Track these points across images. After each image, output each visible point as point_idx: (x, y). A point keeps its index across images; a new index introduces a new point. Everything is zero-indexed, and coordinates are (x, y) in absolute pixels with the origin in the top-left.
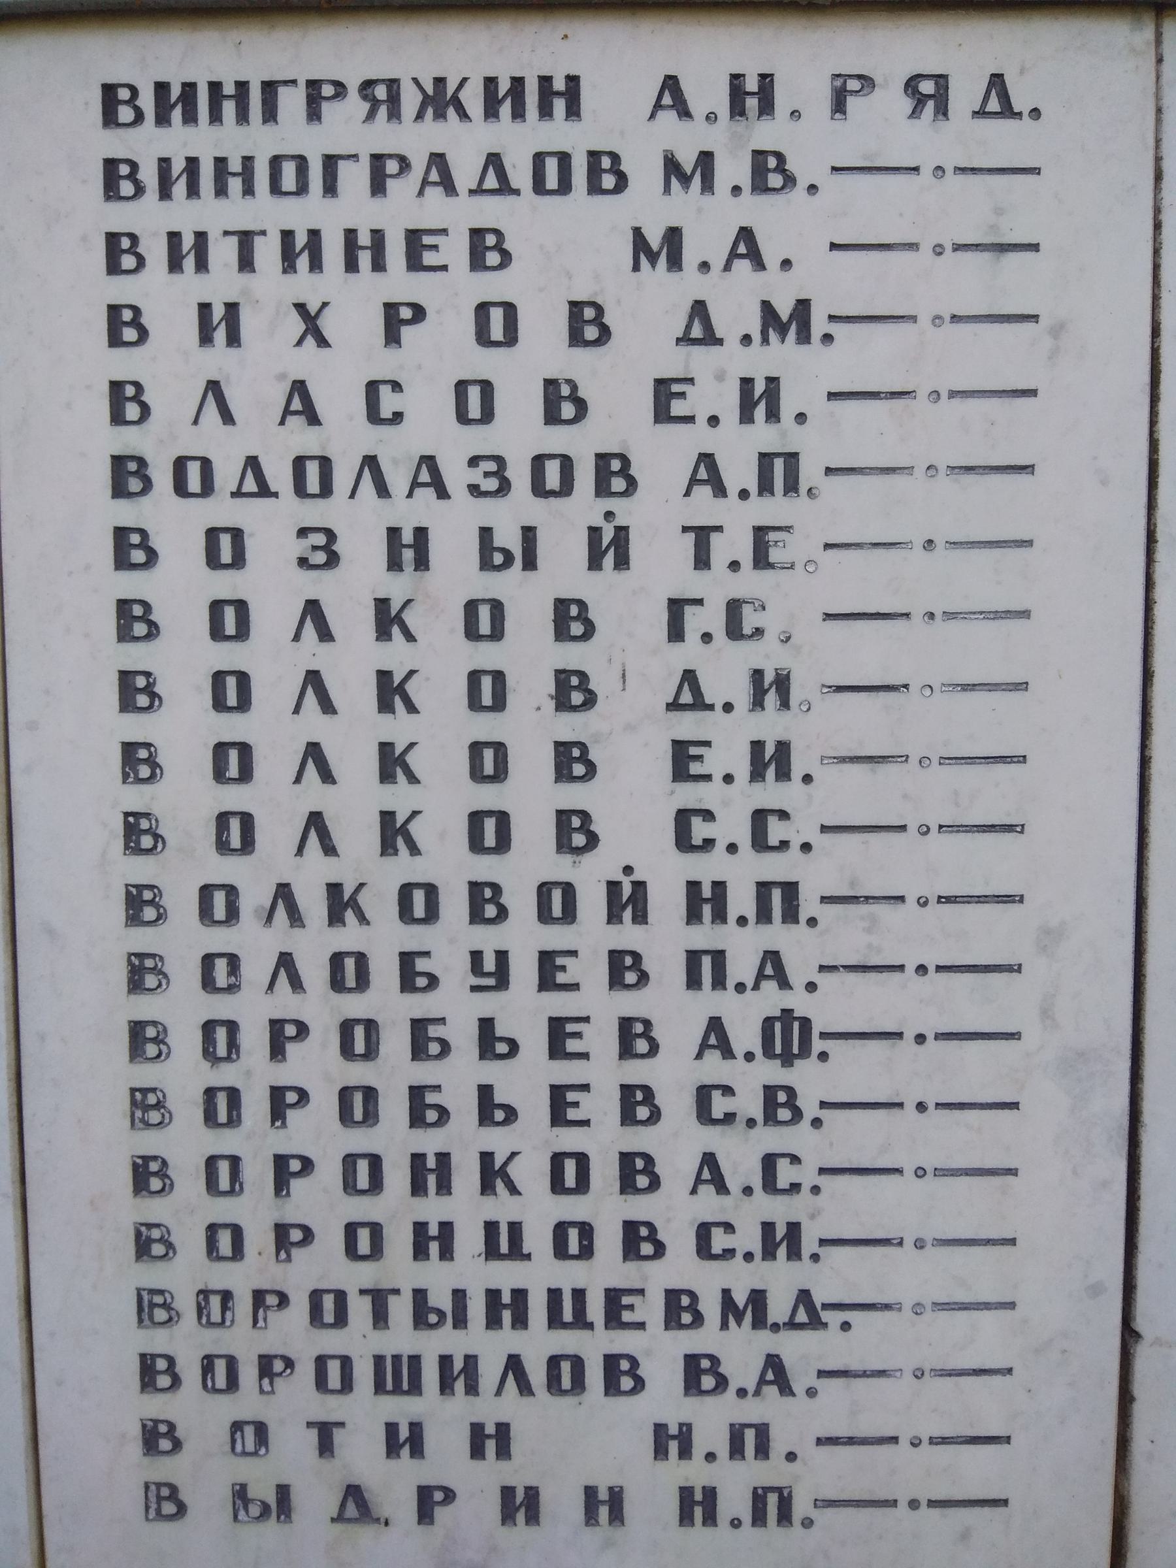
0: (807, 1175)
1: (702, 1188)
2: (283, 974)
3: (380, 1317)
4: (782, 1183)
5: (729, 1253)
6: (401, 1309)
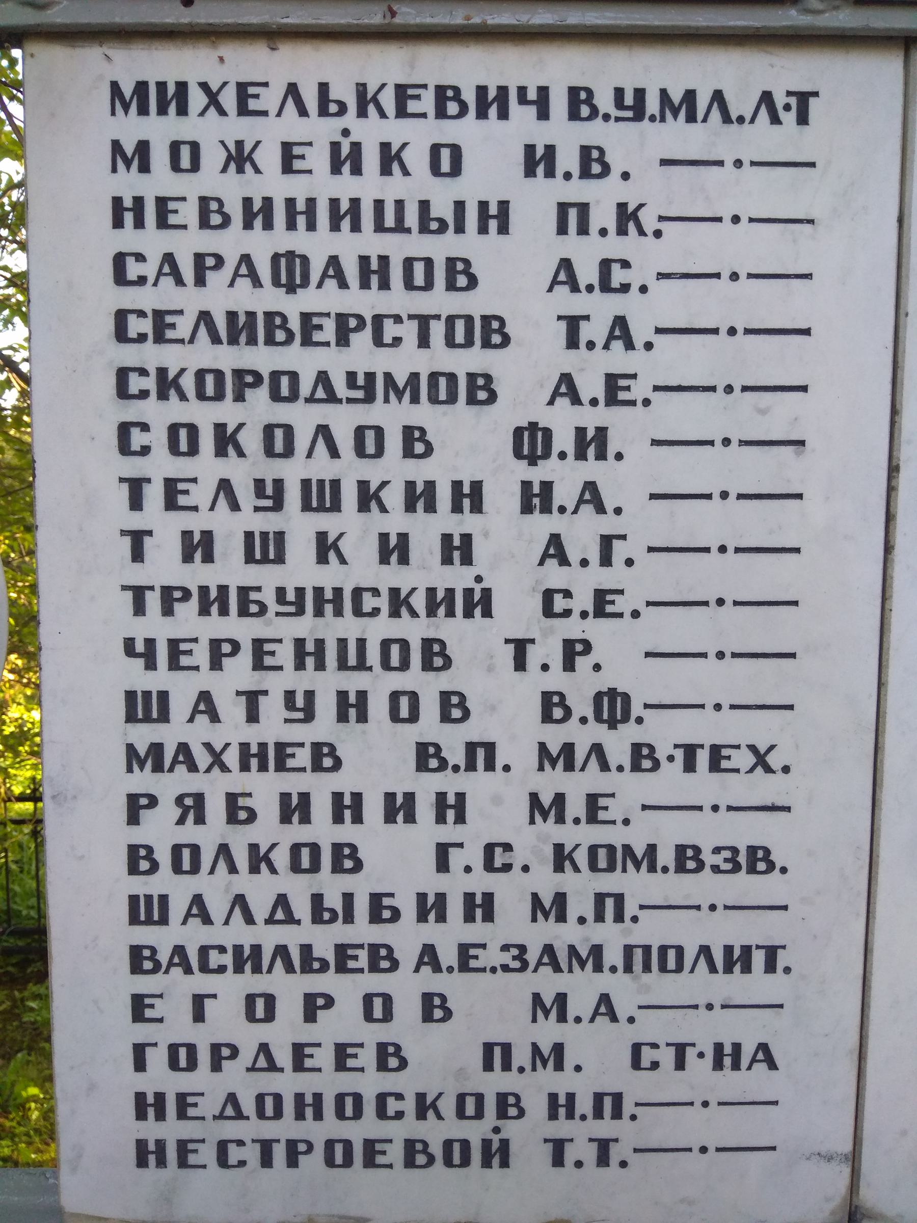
0: (633, 277)
1: (559, 401)
4: (615, 284)
5: (567, 613)
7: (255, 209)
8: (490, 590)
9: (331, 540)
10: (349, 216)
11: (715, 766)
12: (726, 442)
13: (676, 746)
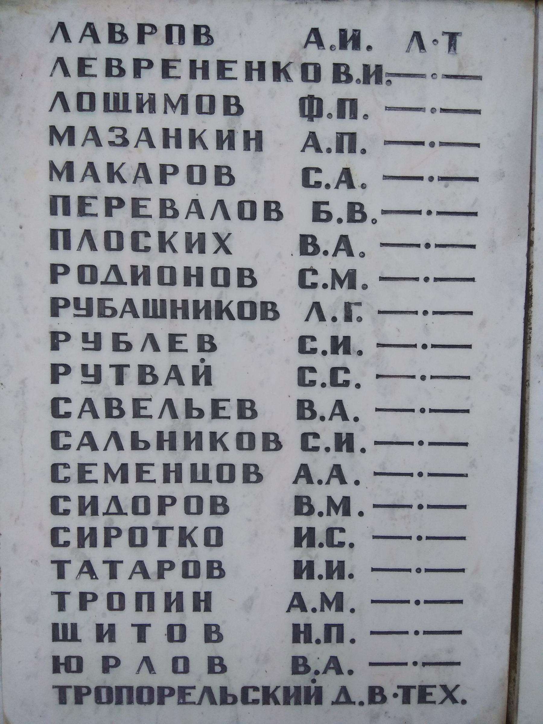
3: (162, 543)
7: (201, 308)
9: (282, 66)
12: (421, 443)
13: (399, 687)
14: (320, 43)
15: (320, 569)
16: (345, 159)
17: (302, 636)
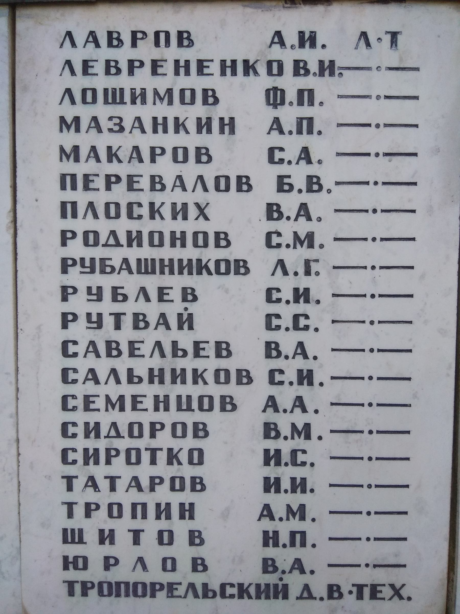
2: (141, 293)
6: (162, 457)
8: (287, 585)
10: (187, 322)
11: (373, 596)
14: (282, 43)
15: (286, 484)
16: (304, 140)
17: (271, 541)
